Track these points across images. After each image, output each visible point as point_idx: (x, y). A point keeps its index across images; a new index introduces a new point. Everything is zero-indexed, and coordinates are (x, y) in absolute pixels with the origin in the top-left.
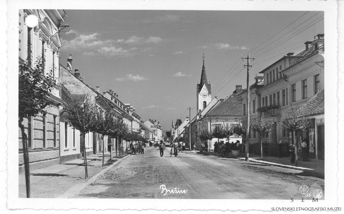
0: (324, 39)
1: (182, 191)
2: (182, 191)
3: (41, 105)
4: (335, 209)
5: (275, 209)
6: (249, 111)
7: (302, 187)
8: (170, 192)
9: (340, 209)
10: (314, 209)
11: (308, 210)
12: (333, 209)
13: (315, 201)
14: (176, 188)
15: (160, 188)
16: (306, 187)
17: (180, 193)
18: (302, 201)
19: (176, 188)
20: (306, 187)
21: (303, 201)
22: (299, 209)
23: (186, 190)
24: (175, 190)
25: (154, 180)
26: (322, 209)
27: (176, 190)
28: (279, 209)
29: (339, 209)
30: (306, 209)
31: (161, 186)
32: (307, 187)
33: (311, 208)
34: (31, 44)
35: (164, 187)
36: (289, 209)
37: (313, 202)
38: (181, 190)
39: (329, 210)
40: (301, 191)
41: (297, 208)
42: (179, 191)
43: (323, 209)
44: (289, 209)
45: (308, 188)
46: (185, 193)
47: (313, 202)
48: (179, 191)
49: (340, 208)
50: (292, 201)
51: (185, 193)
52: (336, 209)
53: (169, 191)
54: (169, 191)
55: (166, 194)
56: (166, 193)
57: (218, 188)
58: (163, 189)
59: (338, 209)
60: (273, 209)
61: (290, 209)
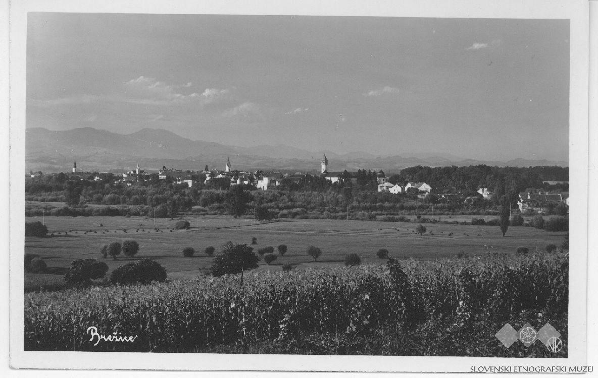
0: (28, 214)
1: (128, 339)
2: (128, 339)
4: (583, 369)
8: (106, 340)
9: (591, 370)
10: (545, 370)
15: (88, 332)
16: (531, 330)
17: (123, 341)
20: (532, 331)
22: (518, 370)
24: (114, 337)
25: (310, 352)
26: (559, 368)
30: (532, 369)
31: (89, 329)
32: (534, 331)
33: (540, 368)
35: (94, 331)
36: (501, 370)
39: (573, 371)
40: (522, 337)
42: (121, 338)
43: (561, 369)
44: (501, 370)
45: (535, 333)
46: (132, 341)
48: (121, 338)
49: (591, 368)
51: (132, 341)
52: (583, 368)
54: (104, 337)
55: (97, 343)
56: (98, 342)
57: (214, 205)
58: (93, 334)
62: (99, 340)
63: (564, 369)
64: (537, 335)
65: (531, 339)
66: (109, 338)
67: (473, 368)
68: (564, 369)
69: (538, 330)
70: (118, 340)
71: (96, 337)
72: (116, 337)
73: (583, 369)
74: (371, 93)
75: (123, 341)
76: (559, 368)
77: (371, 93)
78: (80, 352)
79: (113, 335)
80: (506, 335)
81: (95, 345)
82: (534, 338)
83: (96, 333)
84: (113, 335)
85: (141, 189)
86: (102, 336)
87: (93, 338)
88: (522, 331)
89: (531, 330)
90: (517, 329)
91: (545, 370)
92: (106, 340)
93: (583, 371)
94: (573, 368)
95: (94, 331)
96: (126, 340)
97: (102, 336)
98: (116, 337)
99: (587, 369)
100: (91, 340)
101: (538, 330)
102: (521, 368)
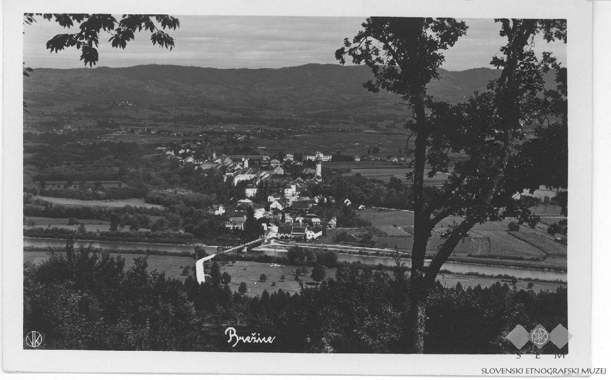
1: (266, 340)
2: (266, 340)
3: (250, 192)
4: (596, 371)
5: (488, 371)
6: (169, 251)
7: (536, 332)
8: (244, 341)
9: (604, 372)
10: (557, 371)
11: (547, 373)
12: (592, 371)
13: (559, 357)
14: (255, 334)
17: (261, 342)
18: (536, 358)
19: (255, 334)
21: (538, 356)
23: (272, 337)
24: (253, 338)
26: (571, 370)
27: (254, 337)
28: (496, 371)
29: (601, 371)
30: (544, 371)
32: (546, 332)
33: (552, 370)
34: (544, 39)
36: (512, 372)
37: (556, 358)
38: (264, 338)
39: (585, 373)
40: (534, 339)
41: (528, 370)
42: (259, 339)
44: (512, 372)
46: (271, 342)
47: (556, 358)
48: (259, 339)
49: (604, 370)
50: (519, 357)
52: (596, 370)
53: (243, 338)
54: (243, 338)
55: (236, 343)
56: (236, 343)
57: (163, 250)
59: (600, 371)
60: (484, 371)
61: (515, 370)
62: (238, 341)
63: (576, 371)
64: (549, 337)
65: (543, 341)
66: (248, 339)
67: (485, 370)
68: (576, 371)
69: (550, 332)
70: (257, 341)
71: (234, 338)
72: (255, 338)
73: (596, 371)
74: (525, 33)
75: (261, 342)
76: (571, 370)
77: (525, 33)
78: (181, 352)
79: (251, 336)
80: (517, 335)
81: (234, 346)
82: (546, 340)
83: (235, 335)
84: (251, 336)
85: (156, 232)
86: (240, 337)
87: (231, 339)
88: (534, 333)
89: (543, 332)
90: (549, 330)
91: (557, 371)
92: (244, 341)
93: (596, 373)
94: (585, 370)
95: (233, 333)
96: (265, 341)
97: (240, 337)
98: (255, 338)
99: (601, 371)
100: (229, 341)
101: (550, 332)
102: (533, 370)
